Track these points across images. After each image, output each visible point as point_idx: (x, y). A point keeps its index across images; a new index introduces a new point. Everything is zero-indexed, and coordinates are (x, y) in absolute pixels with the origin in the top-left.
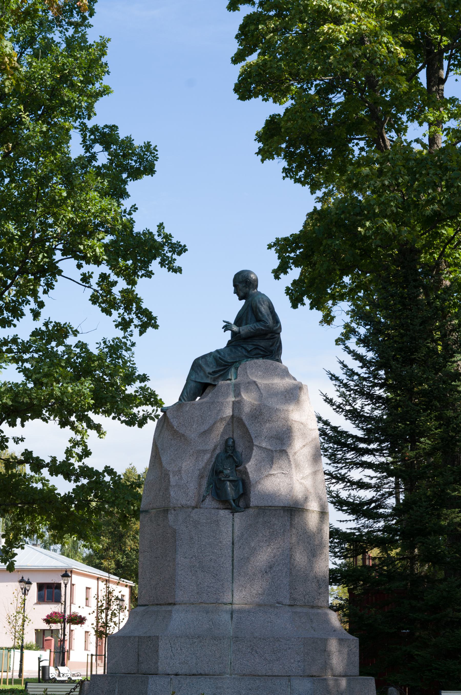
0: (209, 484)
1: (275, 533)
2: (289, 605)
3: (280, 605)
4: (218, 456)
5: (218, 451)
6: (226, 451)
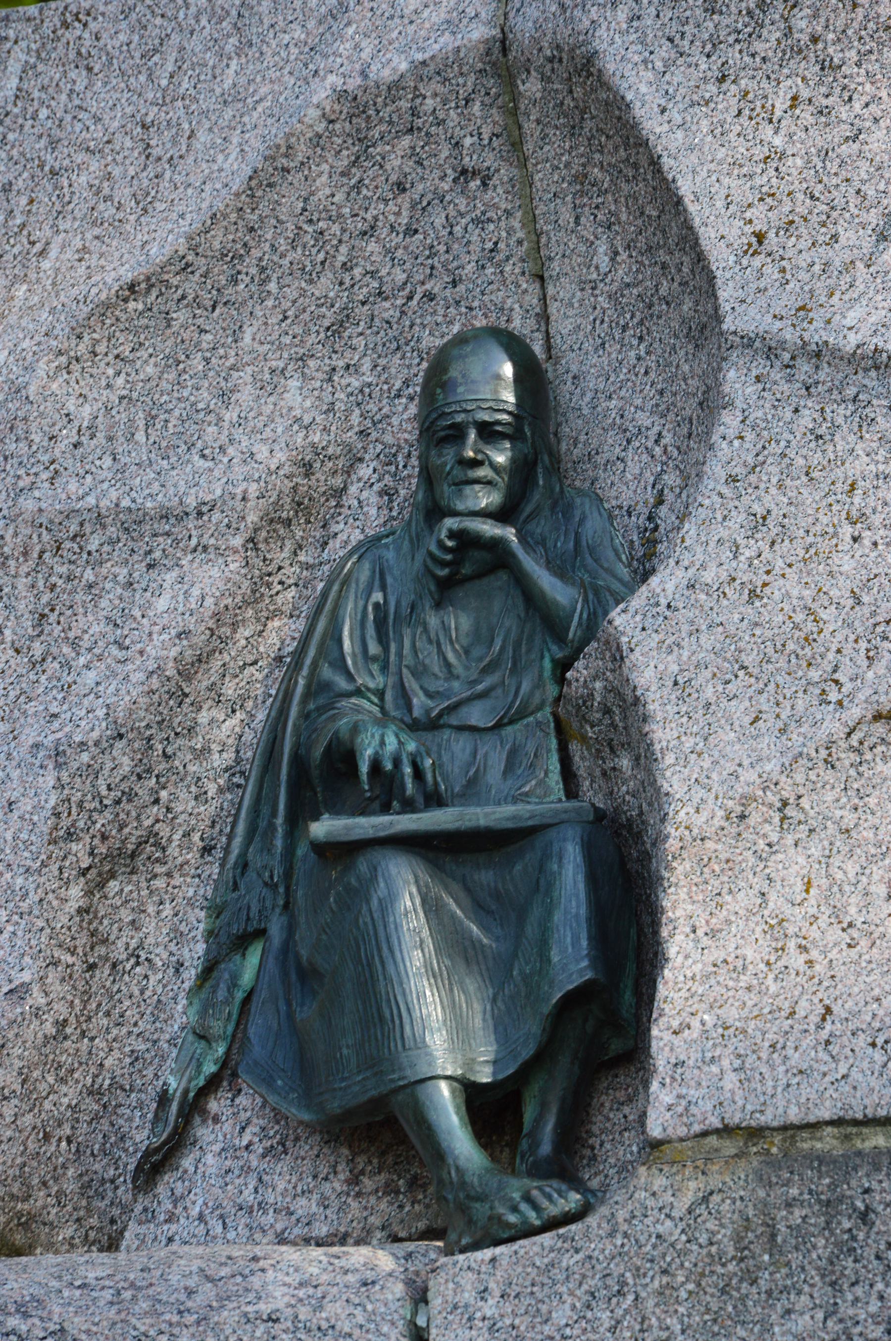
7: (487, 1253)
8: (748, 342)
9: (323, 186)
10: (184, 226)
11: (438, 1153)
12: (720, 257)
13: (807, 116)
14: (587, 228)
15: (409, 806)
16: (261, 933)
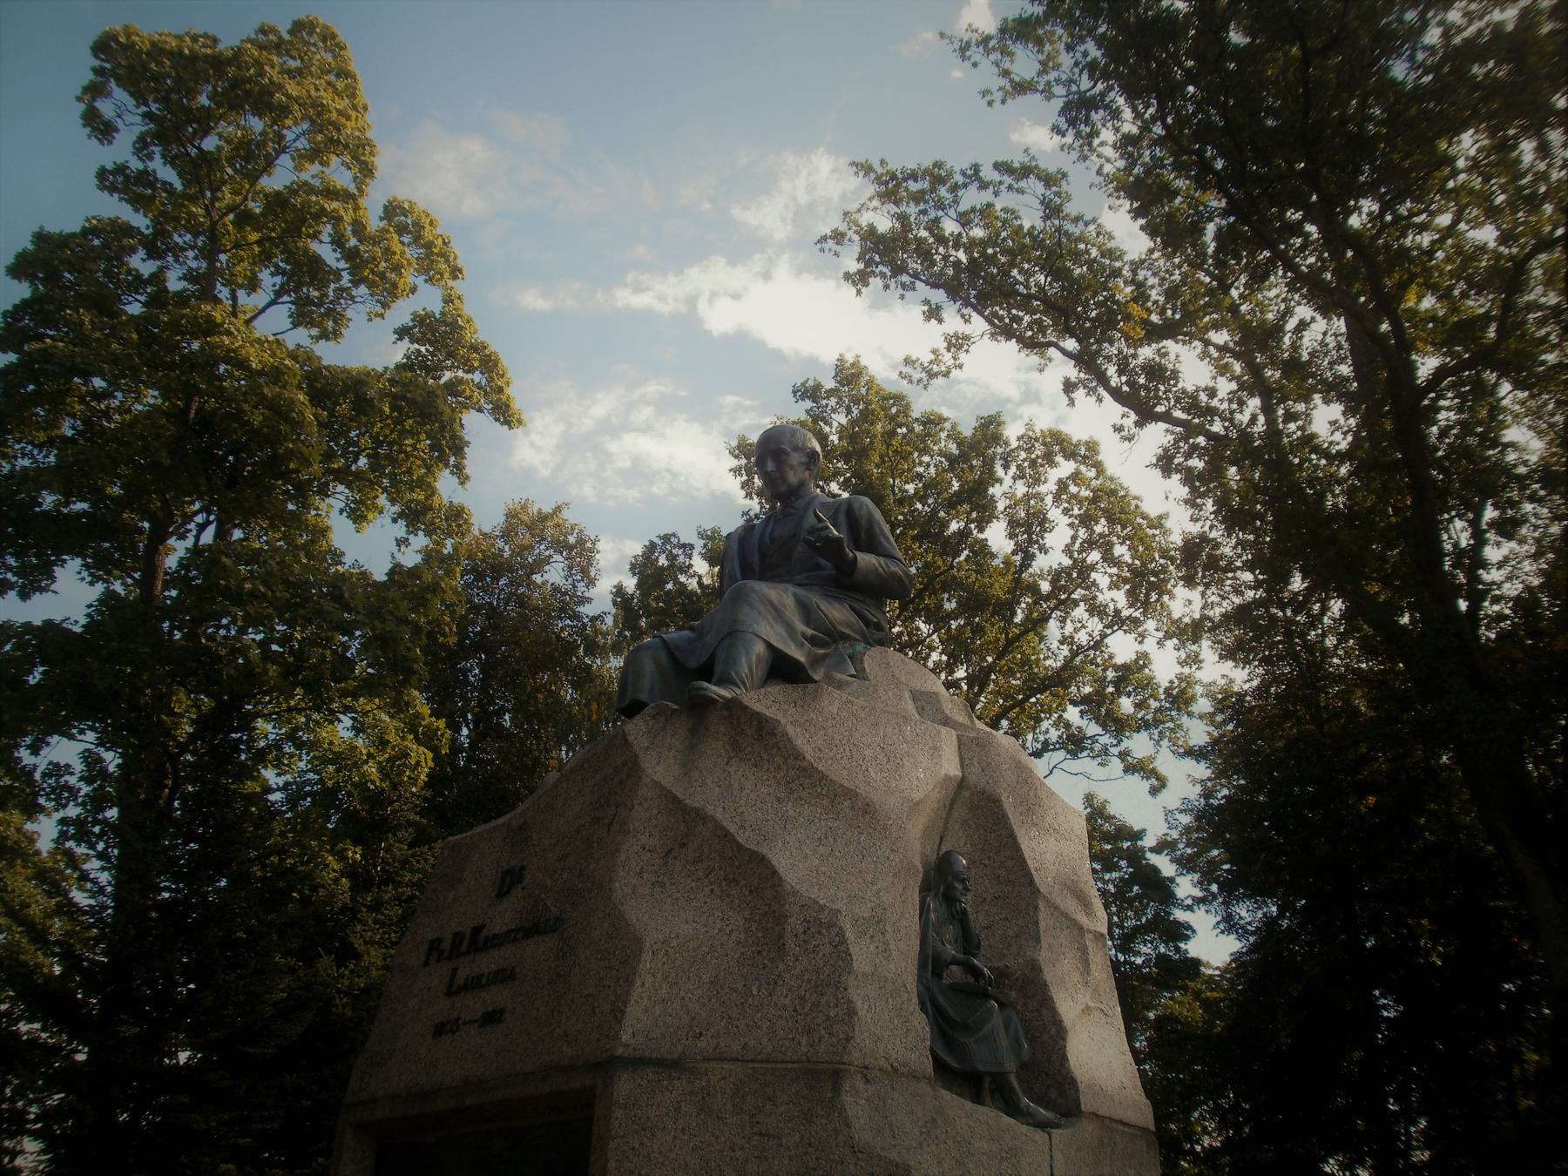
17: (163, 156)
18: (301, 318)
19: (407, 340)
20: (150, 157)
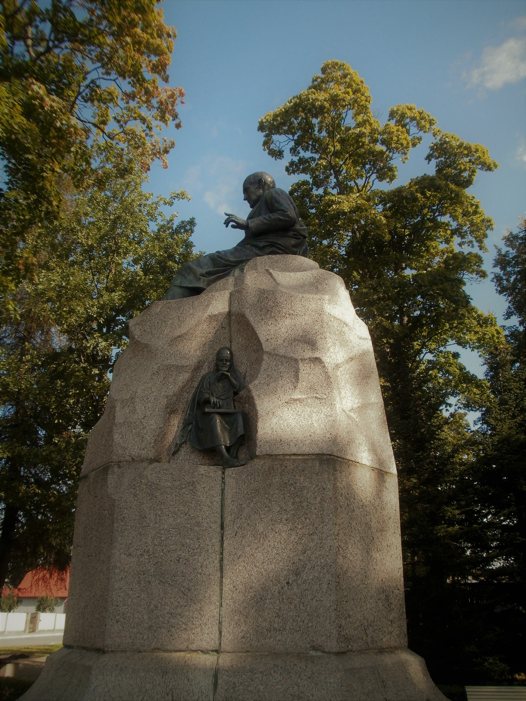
0: (186, 424)
1: (305, 504)
2: (338, 654)
3: (319, 654)
4: (204, 378)
5: (204, 372)
6: (217, 369)
7: (233, 468)
8: (267, 352)
9: (205, 326)
10: (186, 329)
11: (222, 455)
12: (263, 341)
13: (273, 326)
14: (238, 336)
15: (217, 408)
16: (192, 423)
17: (303, 149)
18: (381, 178)
19: (433, 160)
20: (299, 153)
